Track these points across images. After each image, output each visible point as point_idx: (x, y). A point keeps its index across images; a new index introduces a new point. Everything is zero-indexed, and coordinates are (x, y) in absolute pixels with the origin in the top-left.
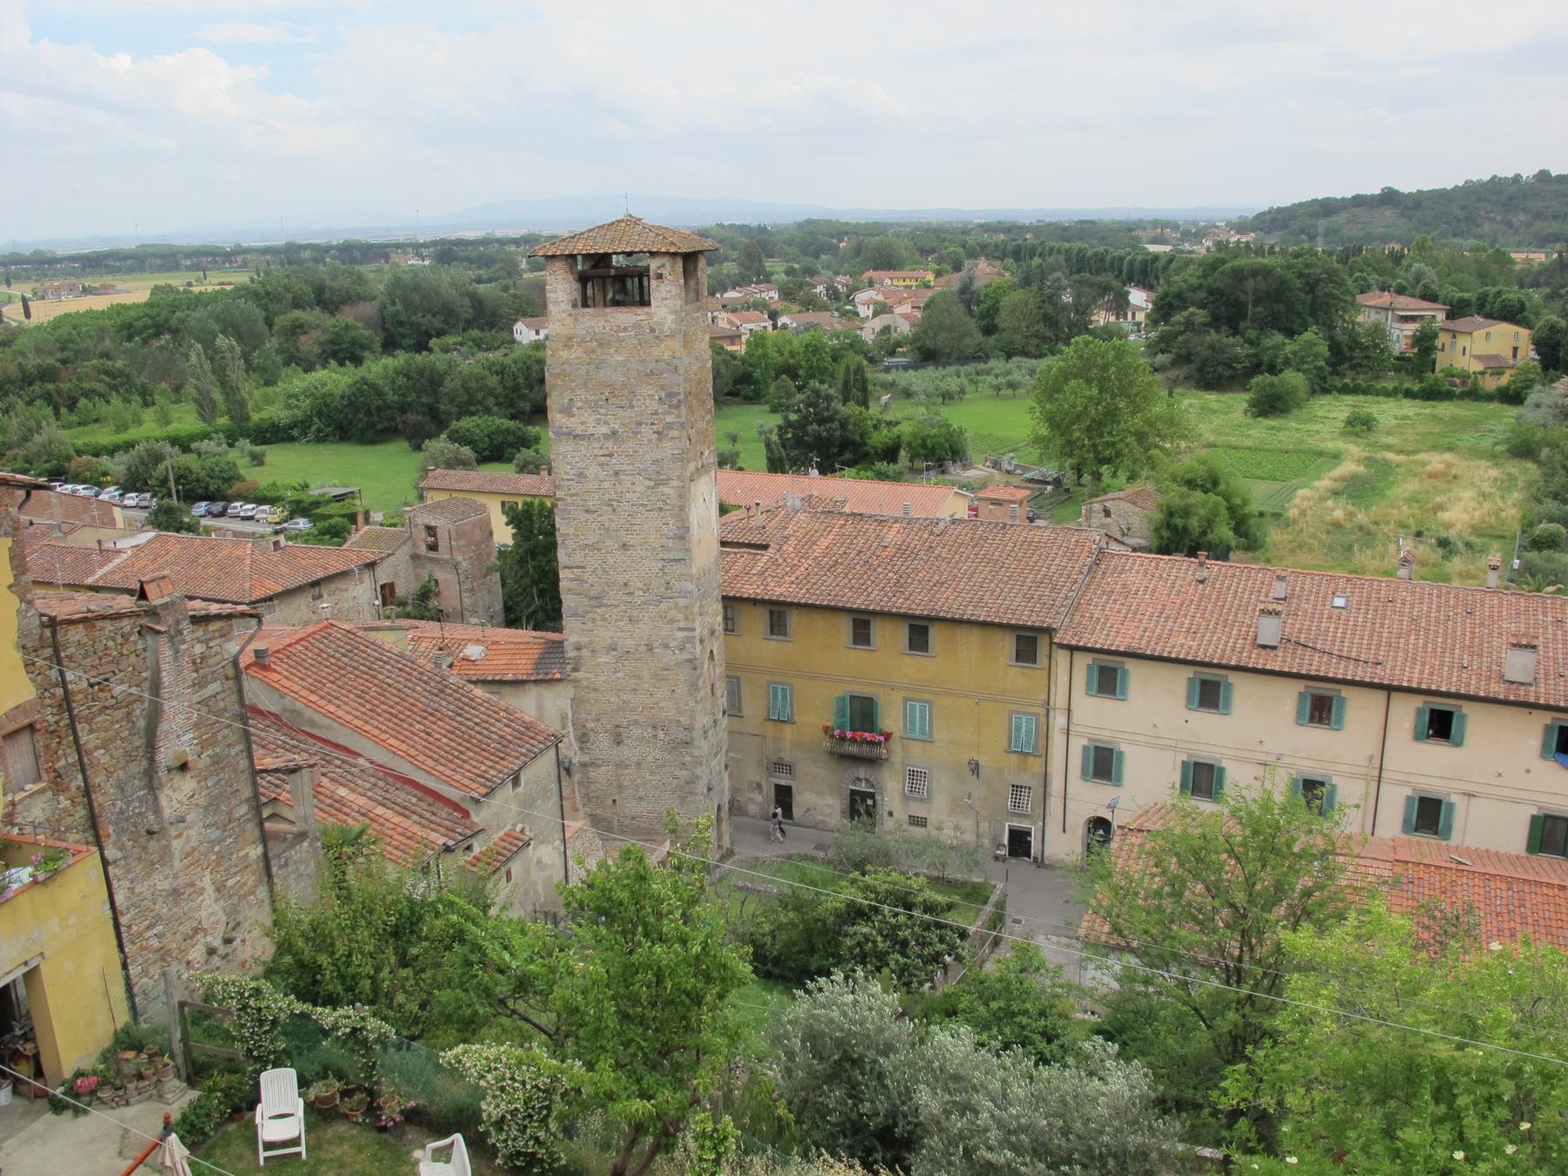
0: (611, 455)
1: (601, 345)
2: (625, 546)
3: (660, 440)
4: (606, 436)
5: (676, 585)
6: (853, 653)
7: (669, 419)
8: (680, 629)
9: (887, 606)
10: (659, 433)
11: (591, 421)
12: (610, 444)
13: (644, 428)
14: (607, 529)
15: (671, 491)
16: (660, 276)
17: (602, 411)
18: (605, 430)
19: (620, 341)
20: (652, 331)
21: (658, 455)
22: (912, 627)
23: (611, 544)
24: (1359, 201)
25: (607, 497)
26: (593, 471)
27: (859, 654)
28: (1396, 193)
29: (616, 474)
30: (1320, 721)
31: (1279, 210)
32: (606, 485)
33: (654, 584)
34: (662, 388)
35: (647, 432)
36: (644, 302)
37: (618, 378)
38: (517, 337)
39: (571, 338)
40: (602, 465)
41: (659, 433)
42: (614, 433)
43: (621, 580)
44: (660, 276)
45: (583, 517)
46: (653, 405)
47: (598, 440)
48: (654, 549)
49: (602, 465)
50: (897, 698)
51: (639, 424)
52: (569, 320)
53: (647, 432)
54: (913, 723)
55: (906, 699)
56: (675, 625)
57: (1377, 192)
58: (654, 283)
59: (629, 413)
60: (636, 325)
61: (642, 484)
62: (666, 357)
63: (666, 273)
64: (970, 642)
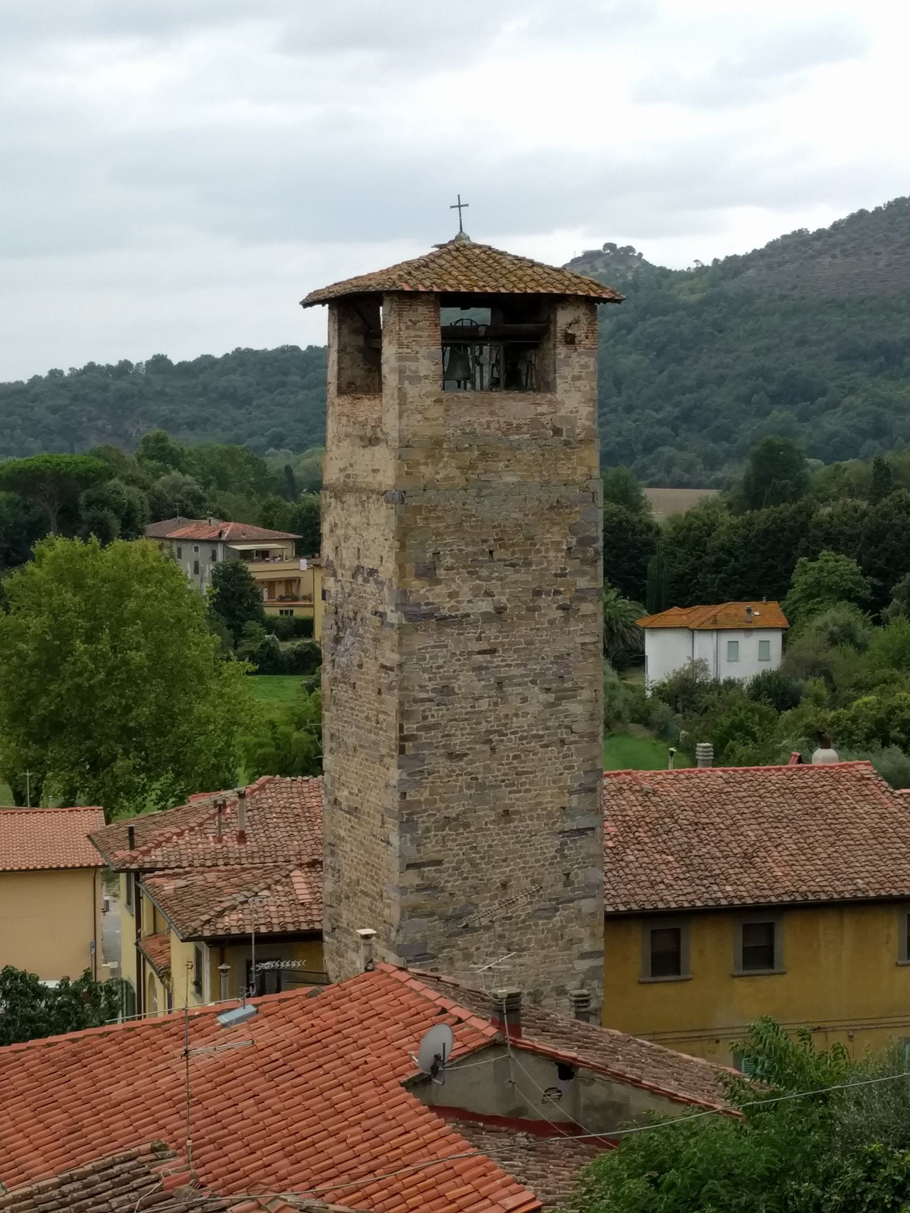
0: (492, 652)
1: (484, 455)
2: (507, 814)
3: (566, 620)
4: (487, 617)
5: (579, 876)
8: (583, 956)
9: (817, 883)
10: (564, 608)
11: (466, 594)
12: (491, 631)
13: (544, 601)
14: (482, 787)
16: (570, 340)
17: (484, 572)
18: (485, 606)
19: (515, 448)
20: (557, 432)
21: (561, 647)
23: (486, 814)
25: (484, 727)
26: (465, 681)
27: (666, 992)
29: (500, 684)
32: (483, 704)
33: (548, 879)
34: (573, 532)
36: (548, 387)
39: (437, 443)
40: (478, 669)
41: (564, 608)
42: (500, 610)
43: (497, 878)
44: (570, 340)
45: (443, 766)
46: (556, 559)
47: (474, 624)
48: (550, 815)
49: (478, 669)
51: (537, 593)
52: (436, 411)
56: (575, 950)
57: (103, 364)
58: (562, 351)
59: (522, 576)
60: (535, 422)
61: (538, 697)
62: (578, 477)
63: (580, 332)
64: (836, 942)
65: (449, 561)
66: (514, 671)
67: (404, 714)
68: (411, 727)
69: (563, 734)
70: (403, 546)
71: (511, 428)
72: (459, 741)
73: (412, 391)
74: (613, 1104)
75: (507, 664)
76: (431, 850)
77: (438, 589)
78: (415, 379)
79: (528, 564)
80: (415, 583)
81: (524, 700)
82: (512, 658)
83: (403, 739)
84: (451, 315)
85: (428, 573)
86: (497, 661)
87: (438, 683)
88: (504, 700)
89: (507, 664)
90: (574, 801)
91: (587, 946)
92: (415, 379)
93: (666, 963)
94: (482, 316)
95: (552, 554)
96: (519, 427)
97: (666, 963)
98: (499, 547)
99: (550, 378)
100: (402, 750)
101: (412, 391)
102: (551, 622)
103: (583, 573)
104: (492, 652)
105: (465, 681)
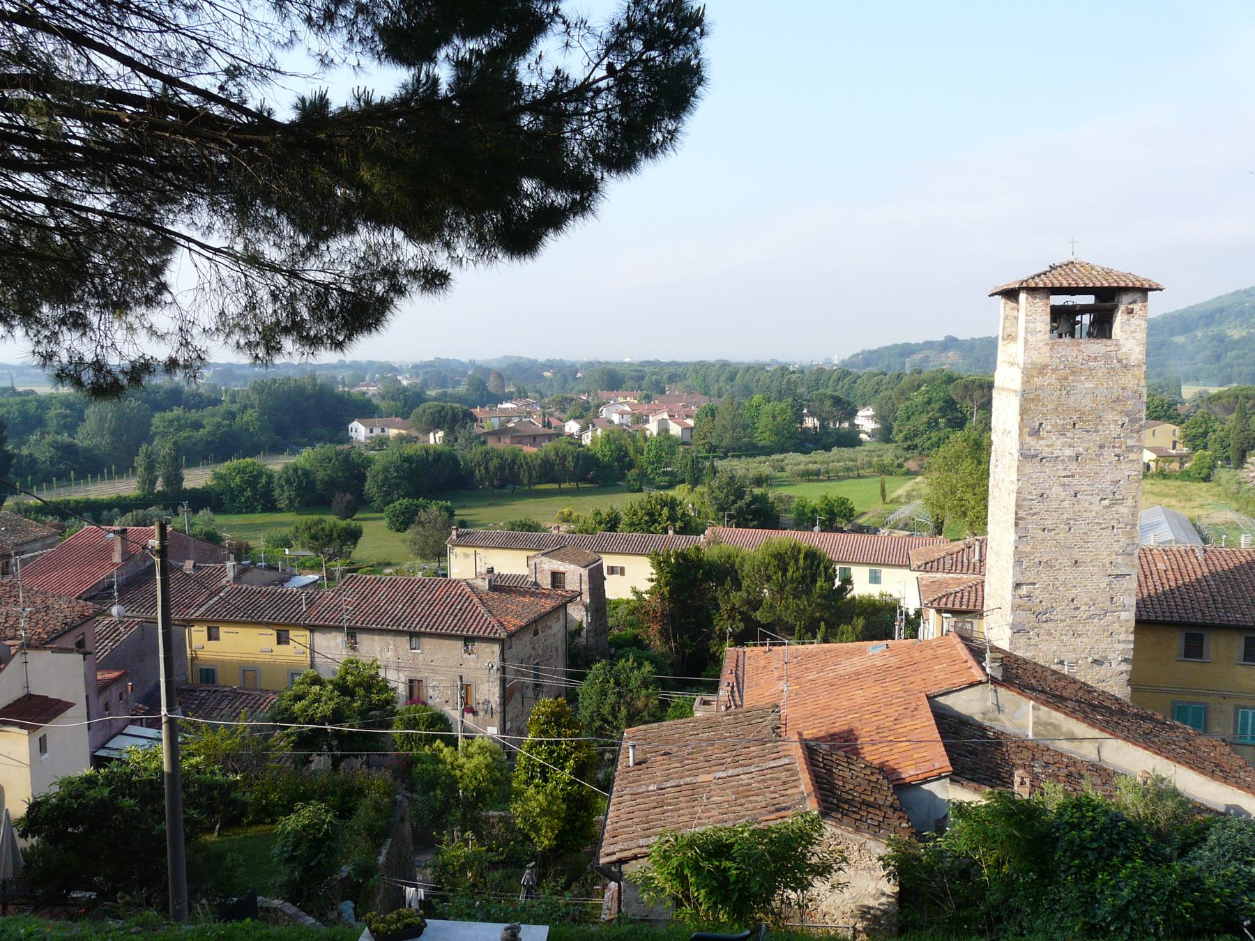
0: (1073, 476)
1: (1073, 373)
6: (1184, 666)
7: (1130, 443)
13: (1105, 451)
15: (1126, 511)
17: (1069, 434)
18: (1069, 452)
22: (1188, 637)
23: (1065, 561)
24: (929, 345)
26: (1056, 490)
27: (1192, 666)
28: (956, 340)
30: (207, 670)
31: (871, 352)
32: (1066, 504)
35: (1109, 455)
37: (1087, 404)
38: (353, 434)
39: (1046, 366)
46: (1115, 430)
50: (1229, 706)
51: (1102, 447)
53: (1109, 455)
54: (1244, 729)
55: (1237, 708)
57: (941, 338)
65: (1049, 428)
66: (1085, 488)
67: (1018, 506)
68: (1022, 514)
69: (1114, 523)
70: (1022, 419)
71: (1090, 358)
72: (1049, 523)
73: (1031, 339)
74: (1051, 724)
75: (1079, 483)
76: (1031, 576)
77: (1041, 442)
78: (1034, 332)
79: (1097, 431)
80: (1028, 439)
81: (1091, 504)
82: (1085, 481)
83: (1017, 519)
84: (1058, 300)
85: (1036, 433)
86: (1075, 482)
87: (1039, 492)
88: (1079, 502)
89: (1079, 483)
90: (1120, 559)
91: (1122, 637)
92: (1034, 332)
93: (1193, 649)
94: (1089, 300)
95: (1112, 427)
96: (1095, 358)
97: (1193, 649)
98: (1080, 421)
99: (309, 368)
100: (1016, 525)
101: (1031, 339)
102: (1110, 463)
103: (1131, 438)
104: (1073, 476)
105: (1056, 490)
